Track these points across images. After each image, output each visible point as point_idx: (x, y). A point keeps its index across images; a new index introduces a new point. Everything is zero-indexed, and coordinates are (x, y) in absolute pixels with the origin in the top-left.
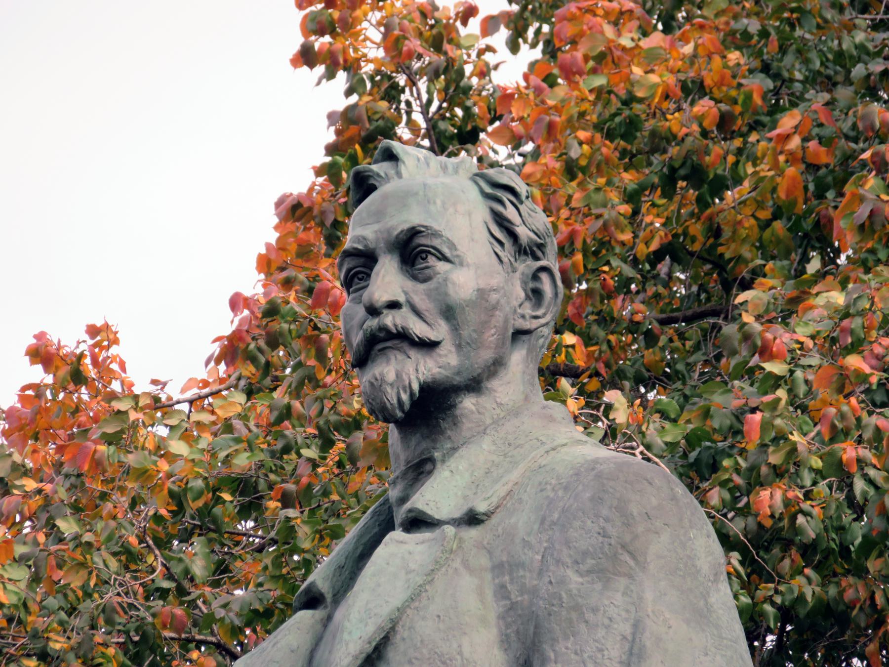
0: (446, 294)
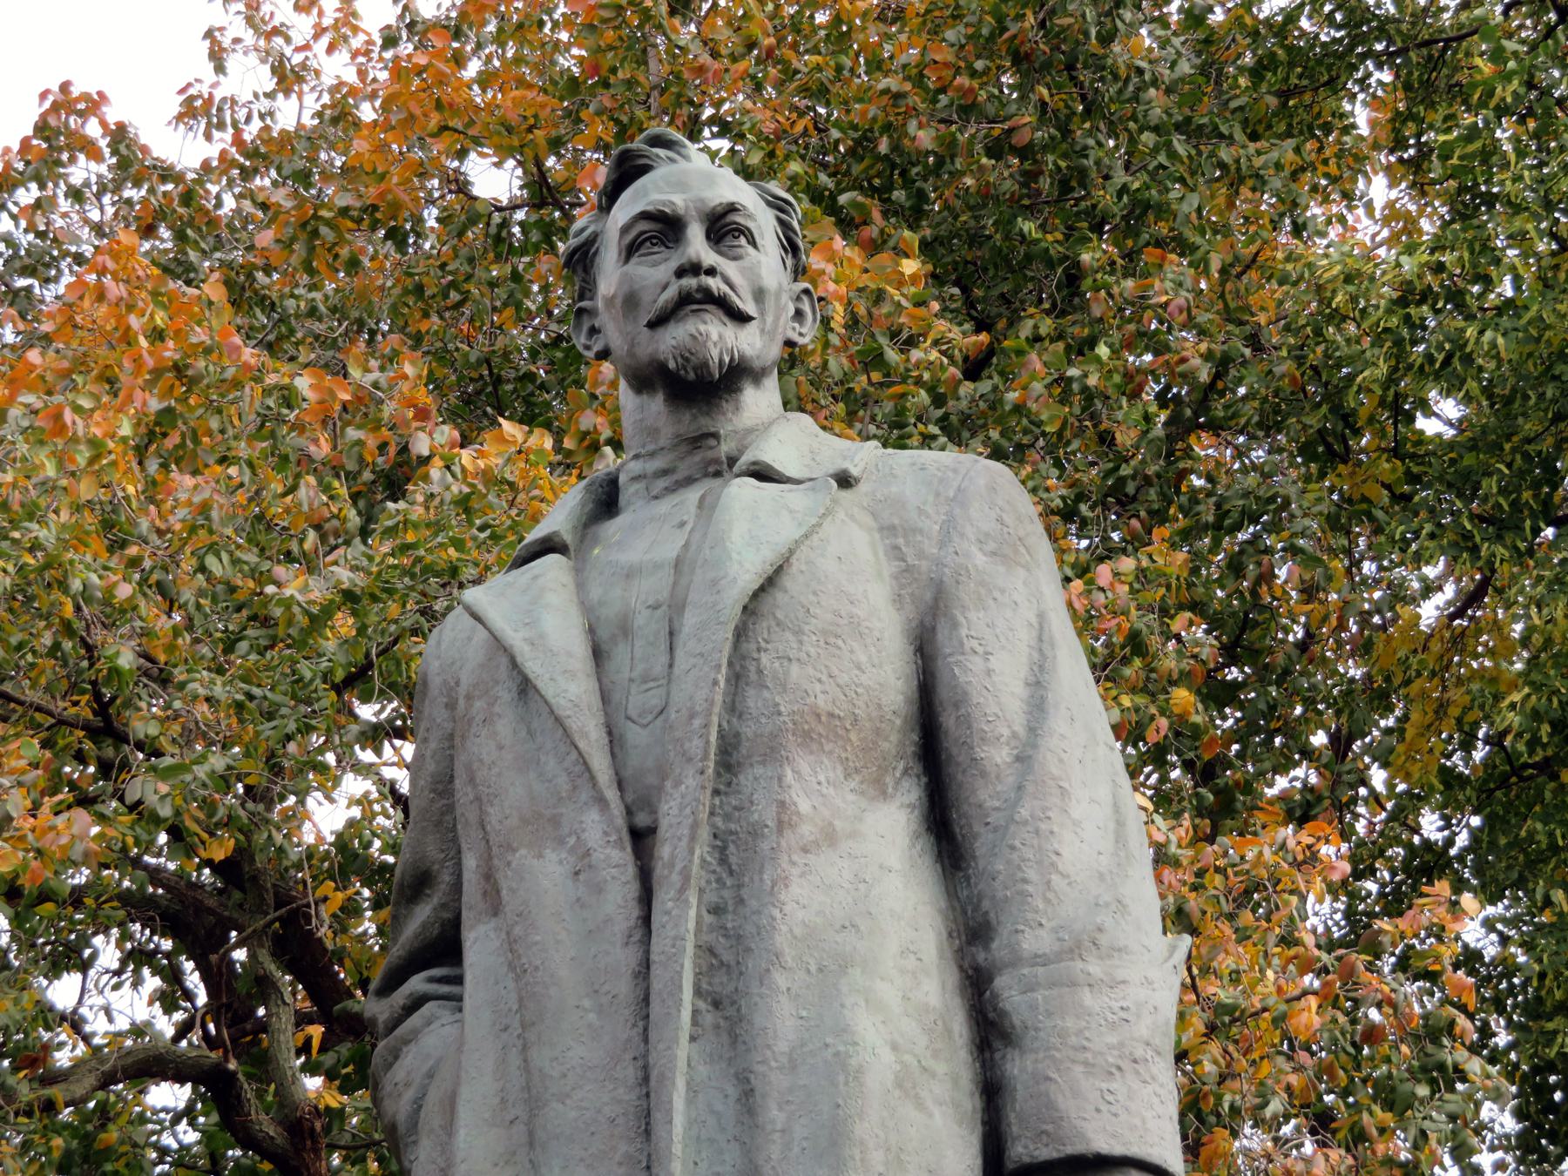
0: (759, 276)
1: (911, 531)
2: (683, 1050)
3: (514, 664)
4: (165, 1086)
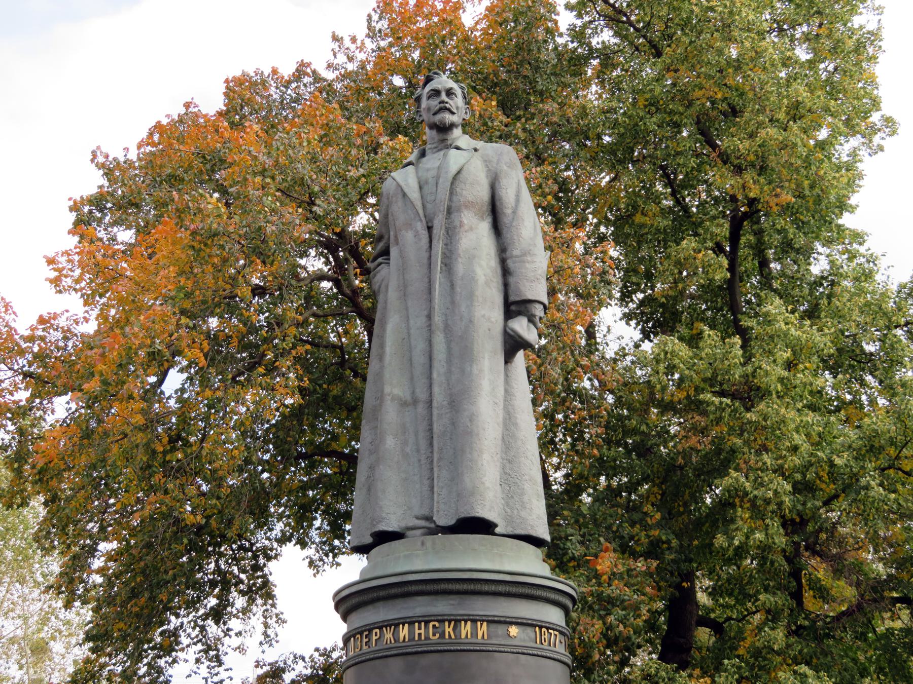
1: (490, 161)
2: (438, 275)
3: (402, 189)
4: (326, 282)
